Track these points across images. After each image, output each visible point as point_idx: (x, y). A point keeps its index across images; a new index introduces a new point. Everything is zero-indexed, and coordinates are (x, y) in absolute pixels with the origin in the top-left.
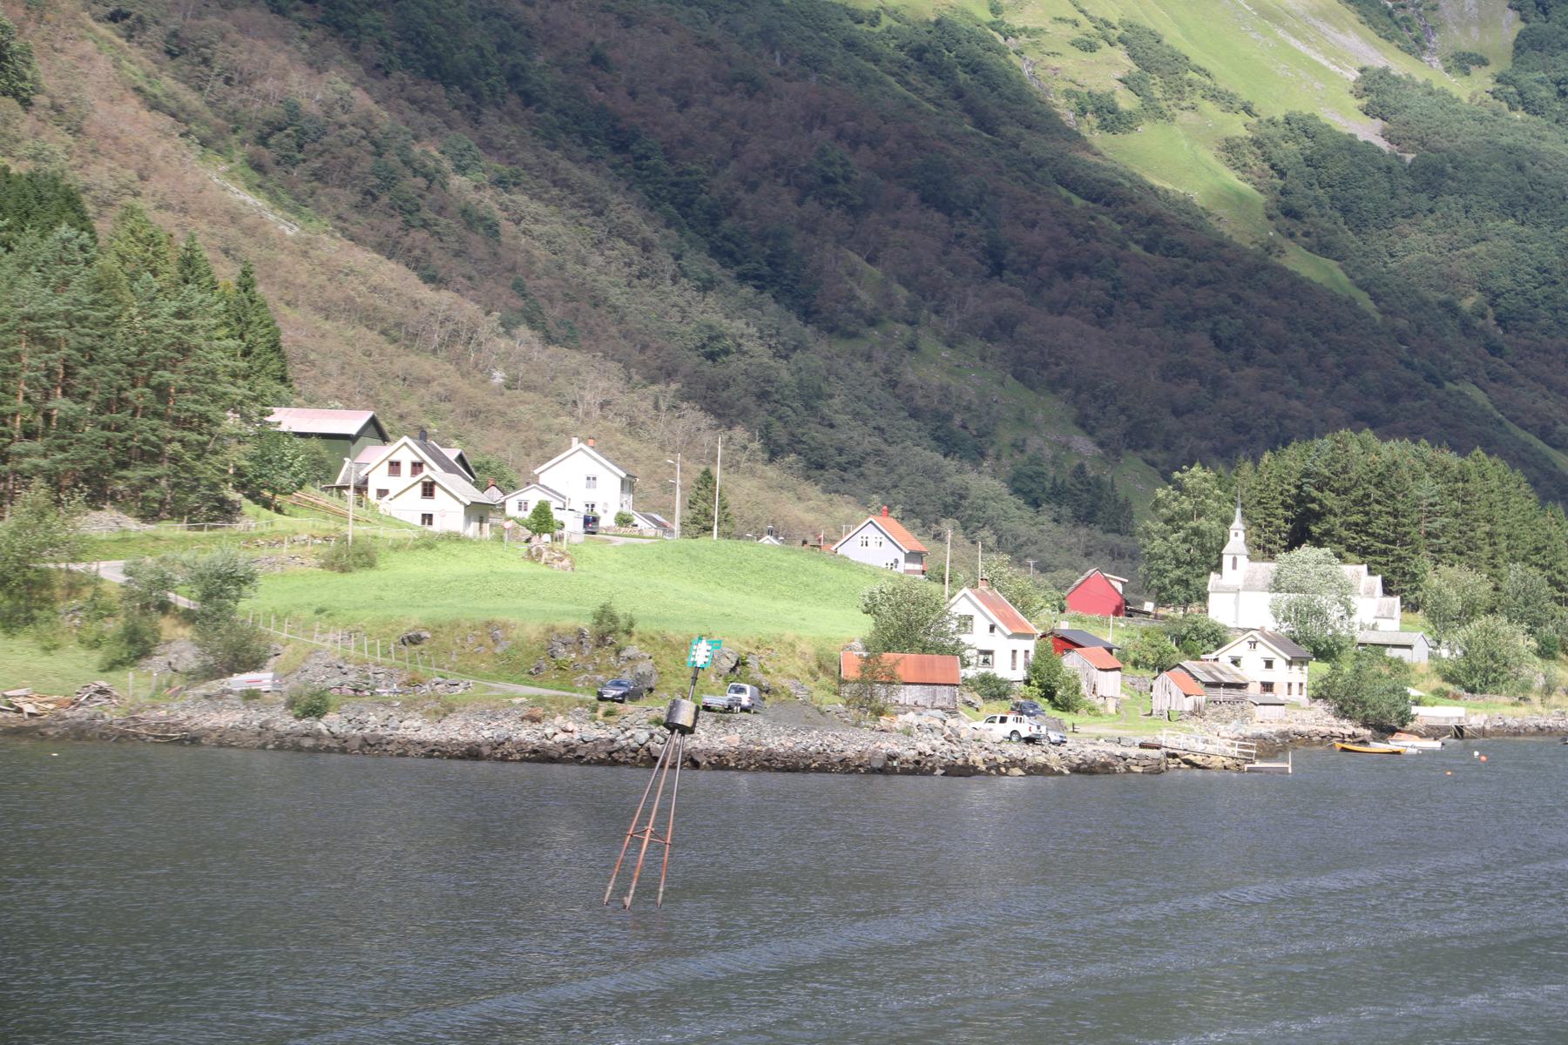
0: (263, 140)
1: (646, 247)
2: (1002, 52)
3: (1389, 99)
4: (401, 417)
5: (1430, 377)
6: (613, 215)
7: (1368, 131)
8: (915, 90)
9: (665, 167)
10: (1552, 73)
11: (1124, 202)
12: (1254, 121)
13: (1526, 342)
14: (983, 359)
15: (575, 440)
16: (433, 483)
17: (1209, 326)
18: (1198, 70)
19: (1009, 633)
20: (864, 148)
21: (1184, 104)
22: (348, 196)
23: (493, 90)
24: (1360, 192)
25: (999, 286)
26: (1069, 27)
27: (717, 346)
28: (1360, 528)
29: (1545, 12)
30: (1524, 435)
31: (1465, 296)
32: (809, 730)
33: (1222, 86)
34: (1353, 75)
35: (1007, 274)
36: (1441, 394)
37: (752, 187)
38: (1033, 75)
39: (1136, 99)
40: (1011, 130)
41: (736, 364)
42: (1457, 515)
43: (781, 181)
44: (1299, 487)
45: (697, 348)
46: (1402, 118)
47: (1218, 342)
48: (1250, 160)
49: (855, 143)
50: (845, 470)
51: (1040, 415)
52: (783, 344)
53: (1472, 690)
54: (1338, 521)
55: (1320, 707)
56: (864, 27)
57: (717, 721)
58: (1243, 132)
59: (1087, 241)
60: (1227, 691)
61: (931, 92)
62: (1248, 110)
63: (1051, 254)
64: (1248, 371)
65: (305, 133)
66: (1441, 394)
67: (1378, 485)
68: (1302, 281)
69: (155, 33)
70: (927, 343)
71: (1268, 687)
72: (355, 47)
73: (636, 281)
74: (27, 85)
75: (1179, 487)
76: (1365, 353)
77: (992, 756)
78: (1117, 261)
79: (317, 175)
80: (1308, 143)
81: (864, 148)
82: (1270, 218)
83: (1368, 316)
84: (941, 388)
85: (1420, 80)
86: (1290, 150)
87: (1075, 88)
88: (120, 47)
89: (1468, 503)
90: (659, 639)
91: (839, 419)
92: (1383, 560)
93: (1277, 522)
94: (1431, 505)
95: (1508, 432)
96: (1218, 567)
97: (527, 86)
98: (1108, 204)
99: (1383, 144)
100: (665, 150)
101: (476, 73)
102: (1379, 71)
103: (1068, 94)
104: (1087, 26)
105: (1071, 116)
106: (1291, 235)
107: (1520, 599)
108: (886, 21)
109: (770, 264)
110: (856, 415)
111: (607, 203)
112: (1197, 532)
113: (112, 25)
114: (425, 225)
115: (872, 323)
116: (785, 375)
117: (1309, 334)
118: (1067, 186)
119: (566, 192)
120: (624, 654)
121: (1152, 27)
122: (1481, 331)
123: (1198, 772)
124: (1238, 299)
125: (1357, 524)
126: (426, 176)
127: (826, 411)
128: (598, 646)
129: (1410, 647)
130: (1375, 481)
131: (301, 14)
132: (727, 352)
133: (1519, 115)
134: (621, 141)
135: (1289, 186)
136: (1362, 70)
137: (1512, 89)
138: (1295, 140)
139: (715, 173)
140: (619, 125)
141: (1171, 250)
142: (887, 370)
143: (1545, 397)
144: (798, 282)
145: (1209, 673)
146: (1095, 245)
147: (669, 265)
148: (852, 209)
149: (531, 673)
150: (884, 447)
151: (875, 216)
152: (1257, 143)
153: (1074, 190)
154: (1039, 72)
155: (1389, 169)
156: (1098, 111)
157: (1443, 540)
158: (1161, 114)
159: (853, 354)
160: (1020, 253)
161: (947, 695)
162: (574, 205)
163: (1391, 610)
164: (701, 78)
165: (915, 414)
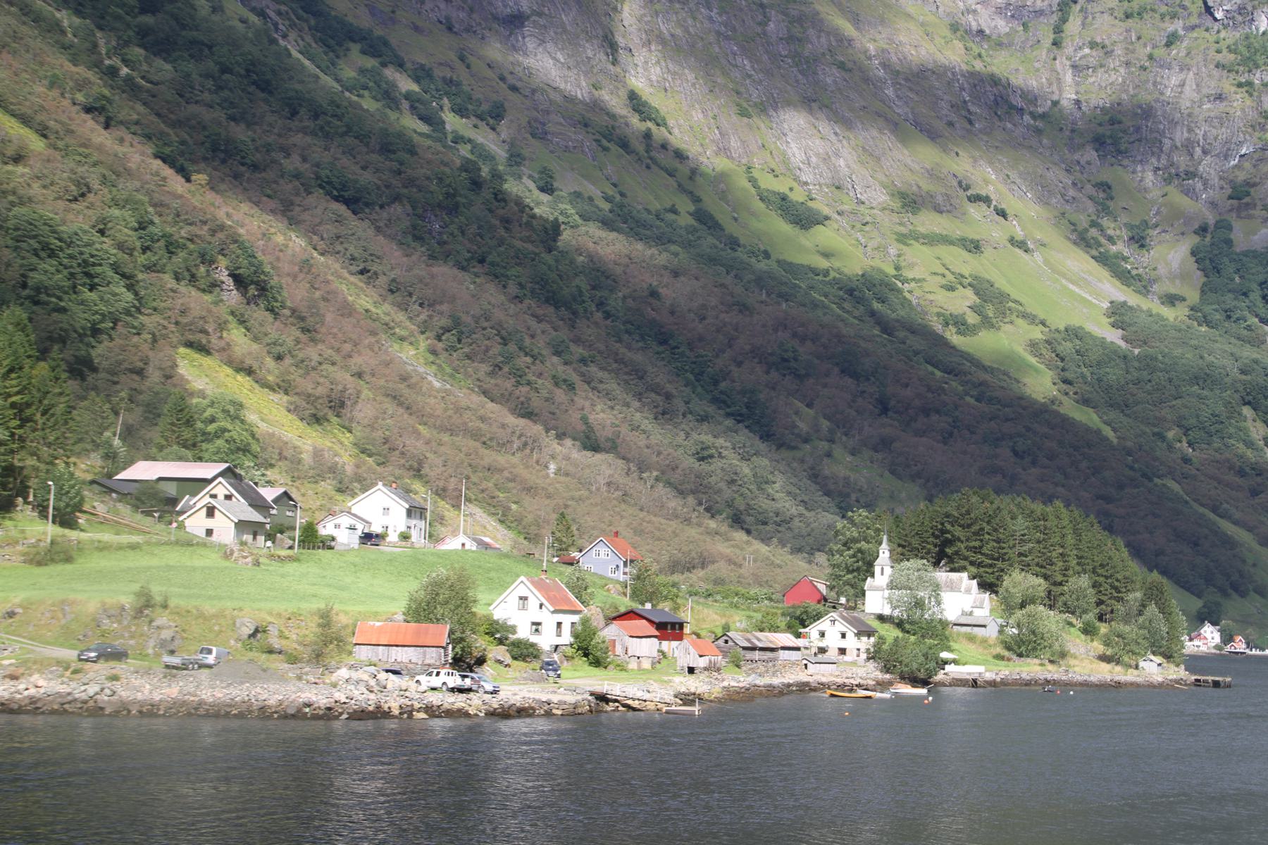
0: (439, 338)
1: (668, 397)
2: (899, 291)
3: (1126, 318)
4: (483, 491)
5: (1144, 475)
6: (649, 379)
7: (1114, 336)
8: (848, 312)
9: (688, 353)
10: (1223, 306)
11: (965, 374)
12: (1047, 329)
13: (1206, 456)
14: (872, 462)
15: (380, 483)
16: (214, 508)
17: (1011, 444)
18: (1015, 302)
19: (552, 609)
20: (809, 343)
21: (1006, 320)
22: (485, 368)
23: (586, 311)
24: (1108, 370)
25: (885, 420)
26: (940, 277)
27: (706, 453)
28: (977, 550)
29: (1218, 272)
30: (1201, 510)
31: (1169, 429)
32: (242, 683)
33: (1029, 310)
34: (1106, 305)
35: (890, 413)
36: (1150, 485)
37: (739, 364)
38: (919, 304)
39: (978, 317)
40: (902, 334)
41: (717, 464)
42: (1039, 542)
43: (756, 360)
44: (942, 524)
45: (694, 455)
46: (1134, 329)
47: (1016, 454)
48: (1044, 352)
49: (803, 339)
50: (780, 525)
51: (903, 495)
52: (747, 452)
53: (1020, 655)
54: (962, 546)
55: (871, 665)
56: (820, 278)
57: (165, 677)
58: (1040, 336)
59: (939, 395)
60: (762, 653)
61: (857, 313)
62: (1043, 323)
63: (917, 402)
64: (1033, 470)
65: (463, 333)
66: (1150, 485)
67: (988, 523)
68: (1068, 419)
69: (382, 280)
70: (838, 451)
71: (842, 651)
72: (504, 287)
73: (660, 417)
74: (278, 304)
75: (851, 521)
76: (1105, 461)
77: (410, 703)
78: (956, 407)
79: (468, 357)
80: (1078, 342)
81: (809, 343)
82: (1054, 384)
83: (1108, 439)
84: (845, 478)
85: (1145, 307)
86: (1067, 347)
87: (942, 311)
88: (361, 288)
89: (1046, 534)
90: (194, 611)
91: (777, 496)
92: (990, 570)
93: (928, 546)
94: (1023, 535)
95: (1191, 508)
96: (873, 576)
97: (608, 308)
98: (956, 375)
99: (1122, 344)
100: (689, 344)
101: (575, 300)
102: (1120, 303)
103: (938, 315)
104: (950, 277)
105: (940, 327)
106: (1067, 394)
107: (1074, 596)
108: (833, 274)
109: (747, 408)
110: (789, 493)
111: (645, 372)
112: (860, 551)
113: (360, 276)
114: (529, 383)
115: (806, 441)
116: (746, 471)
117: (1072, 450)
118: (933, 365)
119: (622, 366)
120: (154, 624)
121: (989, 278)
122: (1180, 449)
123: (631, 714)
124: (1028, 429)
125: (976, 548)
126: (532, 357)
127: (770, 490)
128: (135, 618)
129: (984, 626)
130: (986, 520)
131: (475, 270)
132: (711, 456)
133: (1203, 329)
134: (663, 338)
135: (1066, 367)
136: (1111, 302)
137: (1199, 314)
138: (1071, 340)
139: (717, 356)
140: (663, 330)
141: (991, 400)
142: (812, 468)
143: (1216, 488)
144: (762, 417)
145: (749, 640)
146: (944, 397)
147: (682, 407)
148: (798, 376)
149: (79, 640)
150: (805, 512)
151: (812, 381)
152: (1048, 342)
153: (936, 367)
154: (922, 303)
155: (1125, 357)
156: (956, 324)
157: (1030, 558)
158: (992, 326)
159: (794, 459)
160: (898, 402)
161: (434, 655)
162: (626, 373)
163: (982, 602)
164: (713, 304)
165: (828, 493)
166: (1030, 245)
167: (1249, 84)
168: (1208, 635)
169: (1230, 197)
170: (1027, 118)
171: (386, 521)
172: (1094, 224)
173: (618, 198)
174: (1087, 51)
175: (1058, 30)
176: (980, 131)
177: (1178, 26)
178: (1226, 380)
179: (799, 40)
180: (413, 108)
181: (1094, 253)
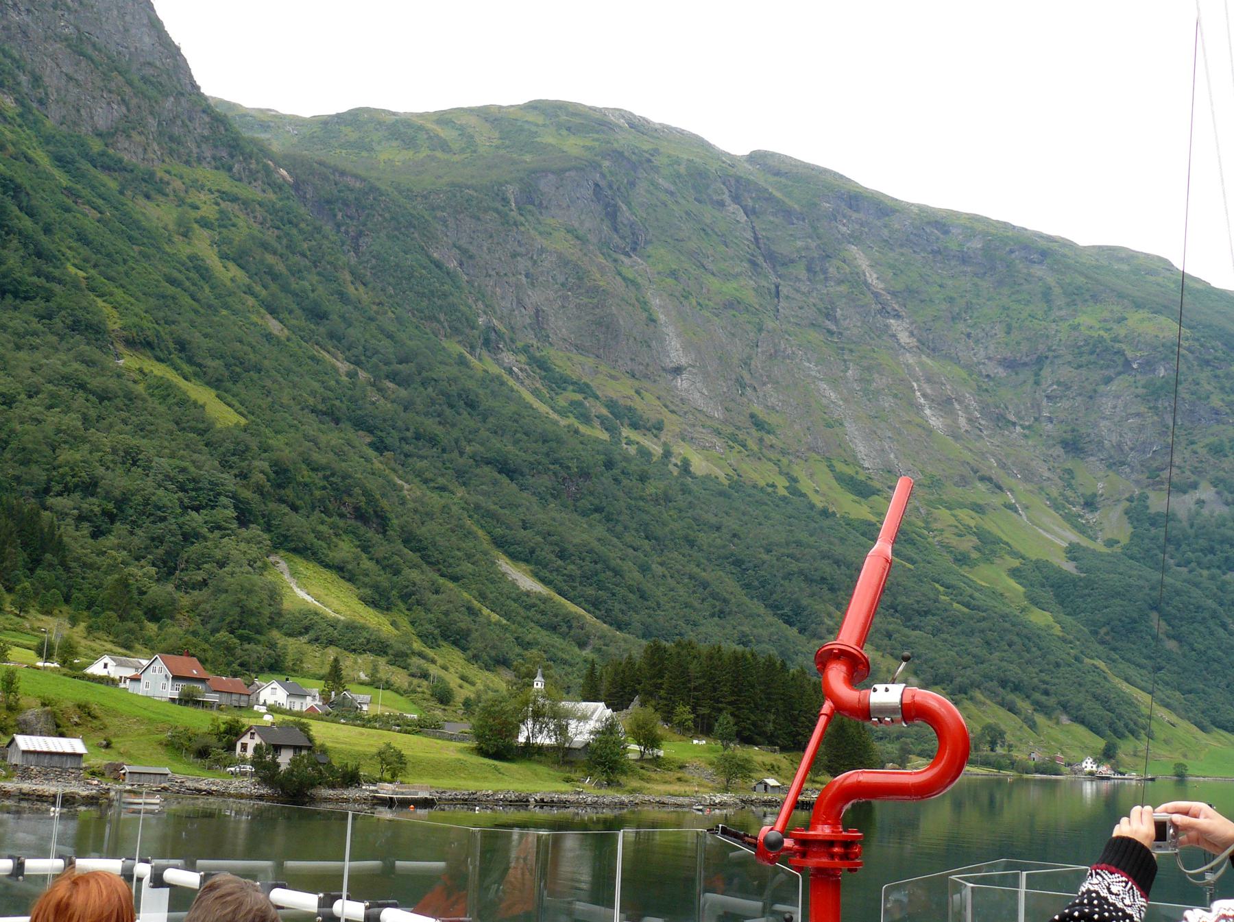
7: (1069, 567)
167: (1157, 408)
169: (1148, 478)
170: (1018, 429)
173: (736, 477)
174: (1055, 387)
175: (1037, 375)
176: (987, 436)
177: (1111, 372)
179: (868, 381)
180: (602, 423)
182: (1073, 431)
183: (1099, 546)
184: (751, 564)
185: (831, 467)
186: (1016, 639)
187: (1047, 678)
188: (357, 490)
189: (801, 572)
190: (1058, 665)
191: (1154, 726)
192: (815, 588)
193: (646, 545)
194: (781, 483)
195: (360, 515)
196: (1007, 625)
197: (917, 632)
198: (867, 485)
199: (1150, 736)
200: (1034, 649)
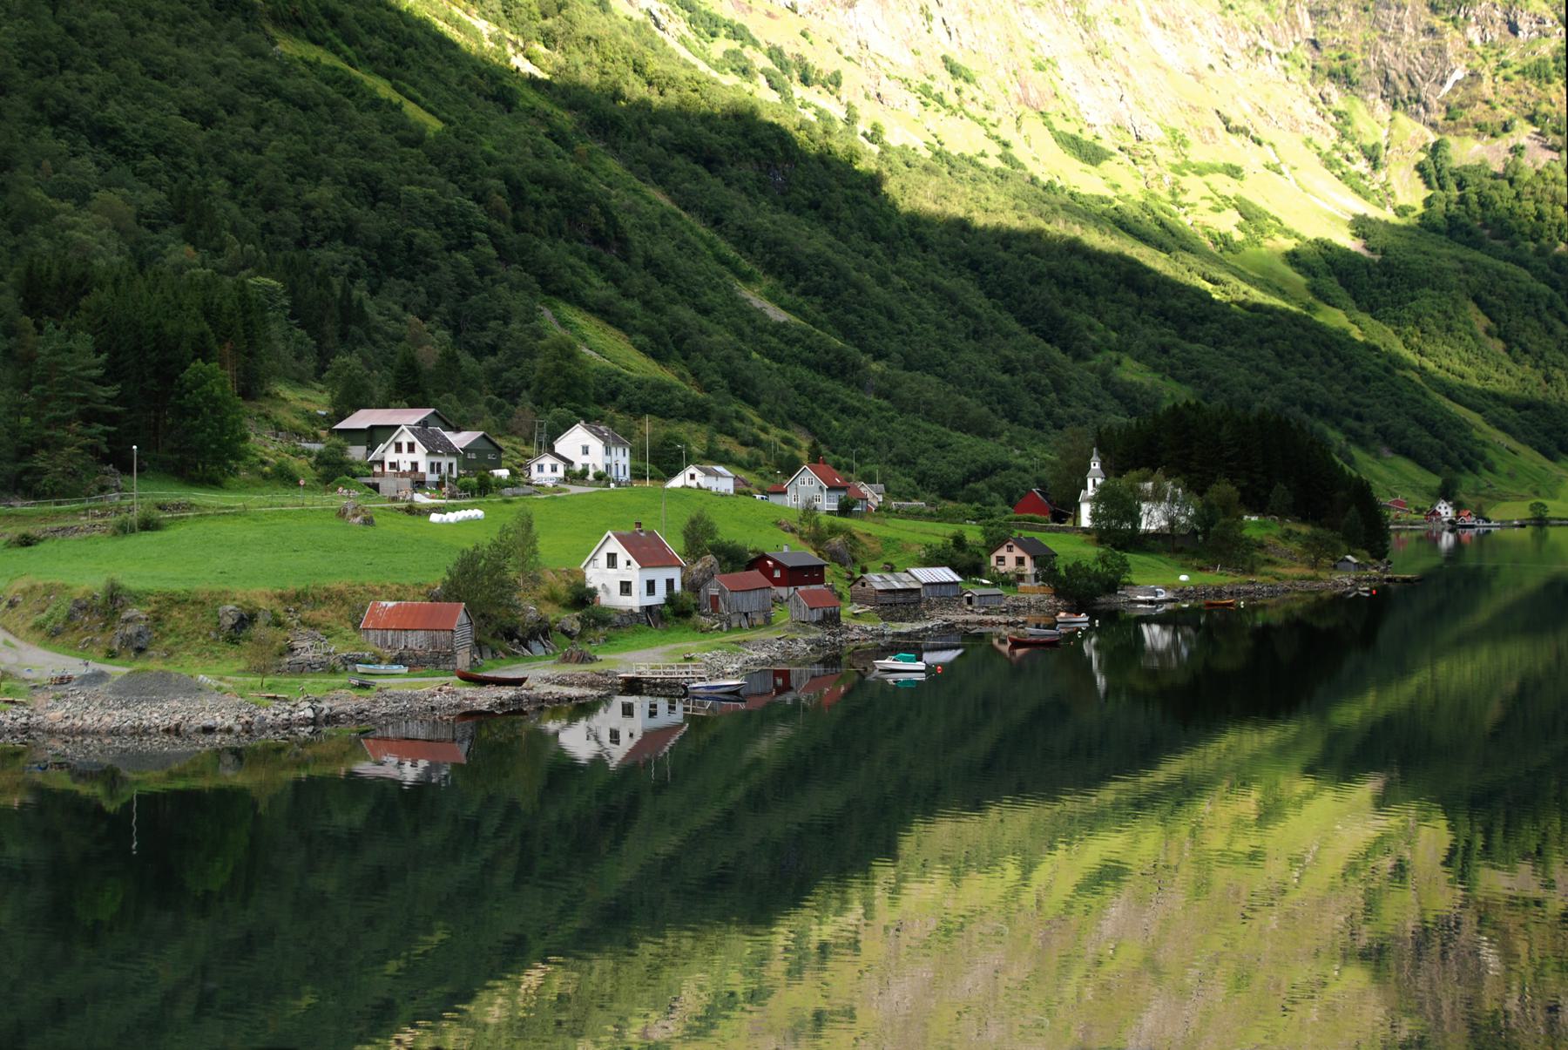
99: (1365, 253)
134: (974, 265)
166: (1283, 168)
168: (1443, 512)
171: (586, 459)
172: (1336, 148)
173: (938, 147)
178: (317, 270)
181: (1338, 172)
182: (1342, 58)
183: (1388, 215)
184: (990, 265)
185: (1049, 126)
186: (1311, 348)
187: (1357, 398)
188: (594, 208)
189: (1051, 274)
190: (1366, 380)
191: (1491, 455)
192: (1070, 293)
193: (877, 248)
194: (994, 149)
195: (599, 239)
196: (1300, 331)
197: (1197, 346)
198: (1096, 148)
199: (1490, 468)
200: (1335, 361)
